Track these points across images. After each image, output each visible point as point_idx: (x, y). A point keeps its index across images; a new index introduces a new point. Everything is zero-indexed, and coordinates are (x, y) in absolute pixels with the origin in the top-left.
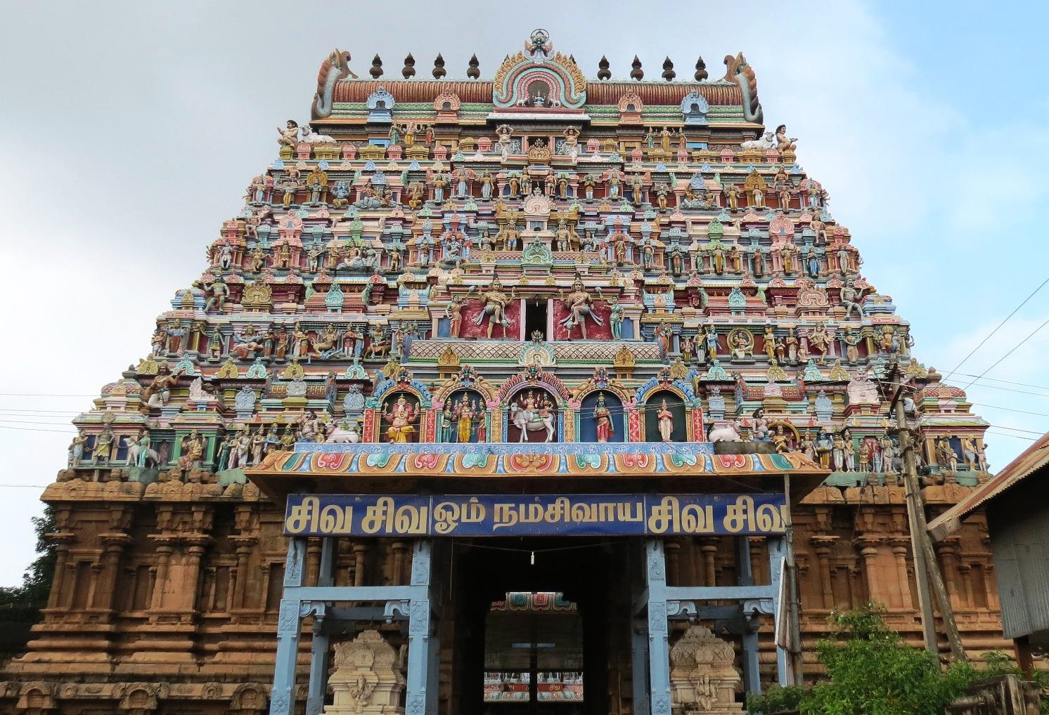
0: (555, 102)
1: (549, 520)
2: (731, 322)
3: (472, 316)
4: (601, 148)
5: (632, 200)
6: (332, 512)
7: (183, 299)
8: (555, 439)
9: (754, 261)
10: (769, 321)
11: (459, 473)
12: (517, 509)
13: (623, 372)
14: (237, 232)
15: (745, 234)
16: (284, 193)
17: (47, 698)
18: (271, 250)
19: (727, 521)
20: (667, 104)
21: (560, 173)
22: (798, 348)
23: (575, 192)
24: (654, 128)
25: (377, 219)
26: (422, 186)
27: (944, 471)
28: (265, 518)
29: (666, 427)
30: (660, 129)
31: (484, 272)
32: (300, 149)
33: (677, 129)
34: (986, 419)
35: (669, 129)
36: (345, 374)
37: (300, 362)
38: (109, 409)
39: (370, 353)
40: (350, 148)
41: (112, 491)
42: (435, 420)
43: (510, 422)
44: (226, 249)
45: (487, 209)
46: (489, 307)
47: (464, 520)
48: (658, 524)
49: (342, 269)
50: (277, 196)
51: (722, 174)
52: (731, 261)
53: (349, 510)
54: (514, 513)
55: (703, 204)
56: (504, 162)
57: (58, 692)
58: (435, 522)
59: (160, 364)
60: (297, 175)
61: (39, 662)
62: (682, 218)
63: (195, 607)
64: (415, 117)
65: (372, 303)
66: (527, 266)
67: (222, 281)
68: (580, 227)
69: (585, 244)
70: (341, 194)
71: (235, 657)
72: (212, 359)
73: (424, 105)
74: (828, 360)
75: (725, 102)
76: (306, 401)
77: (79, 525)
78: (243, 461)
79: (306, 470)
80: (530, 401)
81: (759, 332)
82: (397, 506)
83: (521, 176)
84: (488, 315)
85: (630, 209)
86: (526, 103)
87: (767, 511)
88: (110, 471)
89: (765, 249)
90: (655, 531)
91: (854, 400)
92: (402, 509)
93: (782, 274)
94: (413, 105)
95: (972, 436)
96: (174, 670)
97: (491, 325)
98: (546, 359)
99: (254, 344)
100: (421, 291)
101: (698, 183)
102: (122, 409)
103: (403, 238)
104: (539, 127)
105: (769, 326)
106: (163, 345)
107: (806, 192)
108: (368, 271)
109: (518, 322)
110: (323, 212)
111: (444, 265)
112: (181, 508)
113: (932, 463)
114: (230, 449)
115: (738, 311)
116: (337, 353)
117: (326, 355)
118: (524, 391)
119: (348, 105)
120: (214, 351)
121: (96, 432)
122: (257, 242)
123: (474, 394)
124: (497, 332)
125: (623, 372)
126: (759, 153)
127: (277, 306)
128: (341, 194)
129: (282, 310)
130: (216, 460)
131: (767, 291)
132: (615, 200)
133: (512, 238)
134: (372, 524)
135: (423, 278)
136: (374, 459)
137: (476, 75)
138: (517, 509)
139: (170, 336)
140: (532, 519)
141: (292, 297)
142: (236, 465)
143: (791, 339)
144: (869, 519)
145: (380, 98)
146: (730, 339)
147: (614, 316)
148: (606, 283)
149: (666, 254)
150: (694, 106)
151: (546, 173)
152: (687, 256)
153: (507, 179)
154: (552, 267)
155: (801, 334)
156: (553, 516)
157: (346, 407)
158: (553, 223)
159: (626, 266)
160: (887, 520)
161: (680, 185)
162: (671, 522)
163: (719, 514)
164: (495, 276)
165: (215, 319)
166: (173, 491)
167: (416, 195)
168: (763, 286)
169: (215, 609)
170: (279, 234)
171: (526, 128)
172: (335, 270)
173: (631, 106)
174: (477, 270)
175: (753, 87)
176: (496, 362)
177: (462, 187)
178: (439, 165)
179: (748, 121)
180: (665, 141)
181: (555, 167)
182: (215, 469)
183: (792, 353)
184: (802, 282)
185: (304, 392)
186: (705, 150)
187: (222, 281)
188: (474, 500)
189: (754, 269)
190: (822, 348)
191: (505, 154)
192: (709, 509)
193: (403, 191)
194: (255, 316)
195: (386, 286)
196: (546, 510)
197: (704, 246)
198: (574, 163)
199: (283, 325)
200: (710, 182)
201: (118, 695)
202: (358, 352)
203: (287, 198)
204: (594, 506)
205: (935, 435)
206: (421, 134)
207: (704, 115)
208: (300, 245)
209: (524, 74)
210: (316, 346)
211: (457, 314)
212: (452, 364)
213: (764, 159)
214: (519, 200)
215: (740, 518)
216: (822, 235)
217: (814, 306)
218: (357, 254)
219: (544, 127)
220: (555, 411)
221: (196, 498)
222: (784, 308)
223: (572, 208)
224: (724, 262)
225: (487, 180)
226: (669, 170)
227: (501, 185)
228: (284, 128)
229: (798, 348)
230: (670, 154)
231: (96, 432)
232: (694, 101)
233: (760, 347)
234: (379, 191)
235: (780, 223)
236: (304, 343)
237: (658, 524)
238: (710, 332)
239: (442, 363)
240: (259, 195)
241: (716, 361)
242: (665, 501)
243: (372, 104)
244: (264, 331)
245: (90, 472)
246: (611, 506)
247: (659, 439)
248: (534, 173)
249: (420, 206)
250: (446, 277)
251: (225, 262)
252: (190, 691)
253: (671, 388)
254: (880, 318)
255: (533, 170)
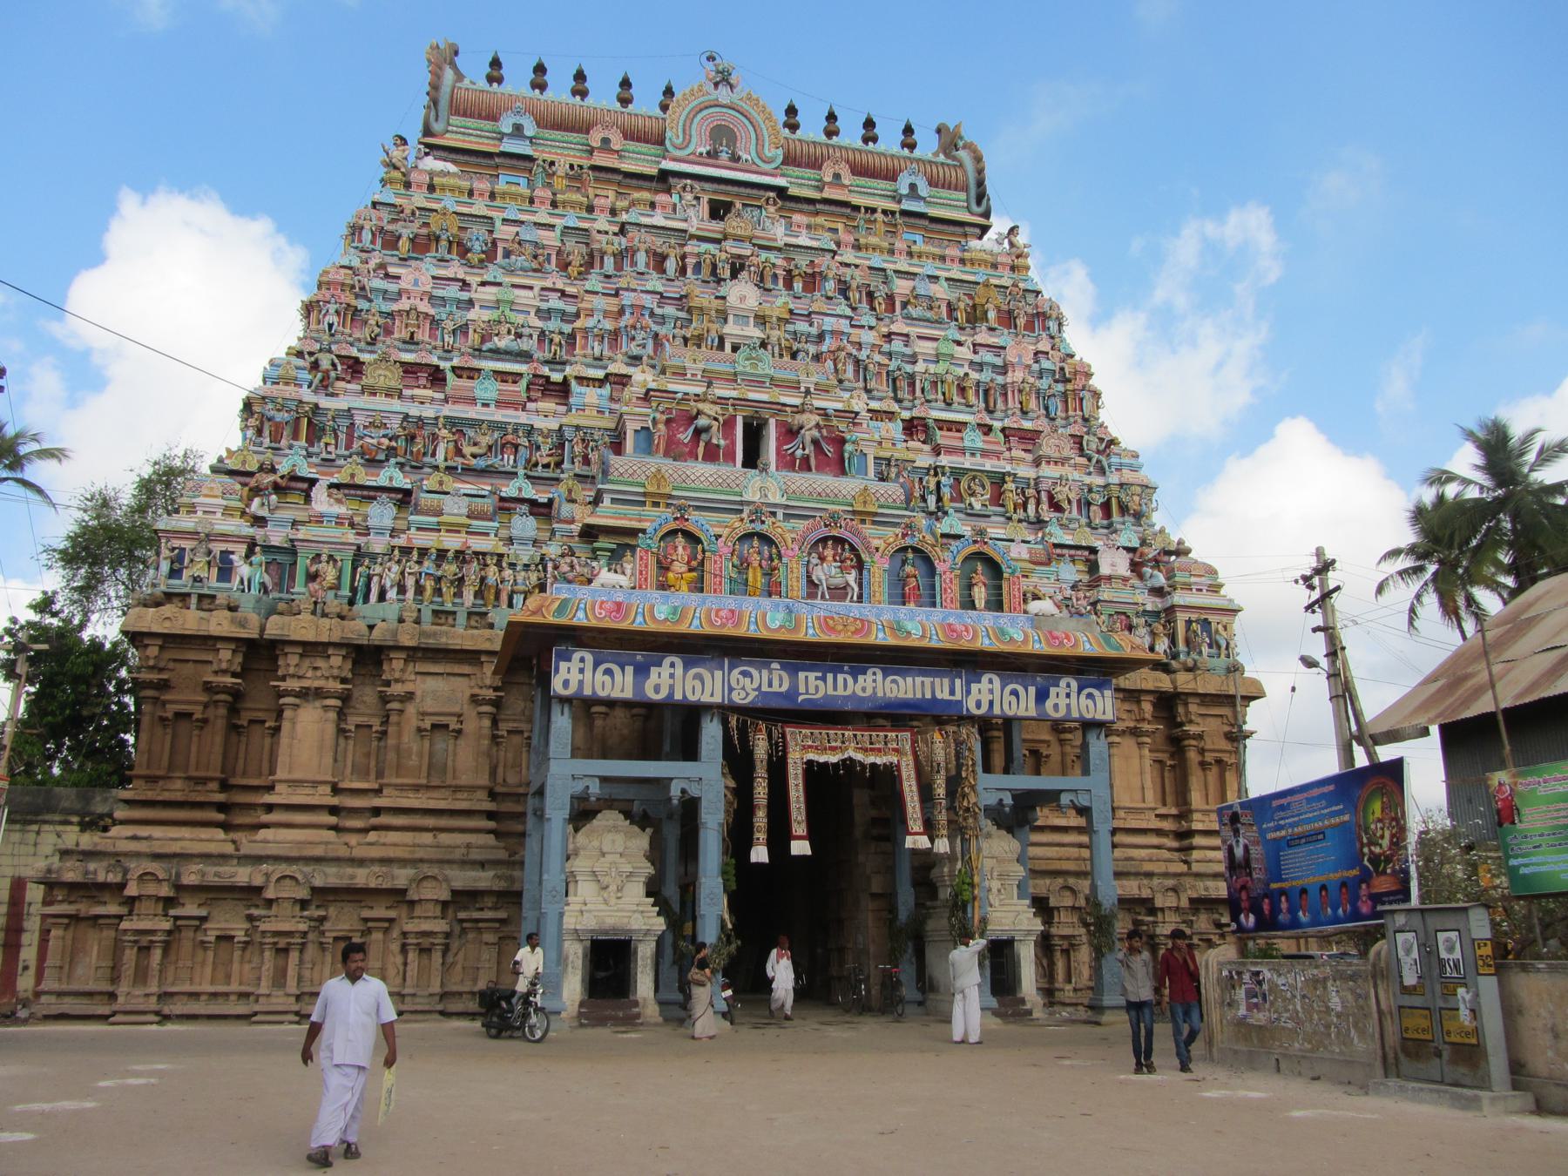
0: (744, 156)
1: (861, 694)
2: (967, 465)
3: (684, 432)
4: (809, 227)
5: (847, 299)
6: (608, 672)
7: (281, 372)
8: (860, 597)
9: (986, 392)
10: (1008, 468)
11: (765, 634)
12: (824, 679)
13: (863, 516)
14: (343, 284)
15: (977, 358)
16: (399, 237)
17: (165, 884)
18: (391, 315)
19: (1049, 704)
20: (471, 116)
21: (764, 255)
22: (1038, 503)
23: (781, 282)
24: (867, 209)
25: (531, 288)
26: (584, 249)
27: (1194, 655)
28: (421, 667)
29: (980, 594)
30: (874, 211)
31: (690, 375)
32: (414, 177)
33: (893, 213)
34: (1238, 601)
35: (885, 212)
36: (510, 489)
37: (450, 470)
38: (200, 514)
39: (536, 465)
40: (482, 185)
41: (219, 624)
42: (721, 564)
43: (809, 576)
44: (332, 308)
45: (673, 291)
46: (702, 422)
47: (765, 688)
48: (978, 705)
49: (490, 351)
50: (391, 242)
51: (947, 279)
52: (962, 390)
53: (629, 670)
54: (820, 683)
55: (929, 314)
56: (693, 231)
57: (178, 875)
58: (731, 689)
59: (261, 457)
60: (413, 214)
61: (135, 838)
62: (905, 330)
63: (223, 772)
64: (563, 152)
65: (530, 399)
66: (743, 374)
67: (330, 351)
68: (790, 327)
69: (798, 351)
70: (477, 247)
71: (393, 837)
72: (324, 455)
73: (573, 137)
74: (1070, 520)
75: (947, 185)
76: (469, 521)
77: (171, 665)
78: (392, 594)
79: (580, 619)
80: (829, 553)
81: (999, 480)
82: (686, 667)
83: (717, 252)
84: (698, 432)
85: (848, 312)
86: (708, 153)
87: (1090, 696)
88: (213, 597)
89: (1000, 379)
90: (975, 712)
91: (1105, 570)
92: (890, 678)
93: (1018, 413)
94: (557, 135)
95: (1225, 619)
96: (318, 851)
97: (702, 444)
98: (774, 495)
99: (386, 441)
100: (599, 391)
101: (924, 288)
102: (219, 515)
103: (565, 317)
104: (723, 187)
105: (1009, 474)
106: (259, 432)
107: (1044, 314)
108: (525, 356)
109: (733, 443)
110: (456, 269)
111: (626, 359)
112: (312, 649)
113: (1182, 647)
114: (370, 578)
115: (973, 453)
116: (493, 461)
117: (481, 463)
118: (824, 540)
119: (470, 122)
120: (327, 444)
121: (188, 545)
122: (370, 301)
123: (765, 539)
124: (712, 455)
125: (863, 516)
126: (988, 257)
127: (407, 392)
128: (477, 247)
129: (412, 397)
130: (354, 590)
131: (1003, 430)
132: (830, 298)
133: (713, 334)
134: (657, 689)
135: (600, 374)
136: (662, 612)
137: (583, 94)
138: (824, 679)
139: (269, 420)
140: (840, 692)
141: (423, 382)
142: (382, 597)
143: (1031, 492)
144: (293, 660)
145: (606, 134)
146: (964, 484)
147: (848, 447)
148: (840, 406)
149: (1038, 392)
150: (913, 187)
151: (748, 253)
152: (911, 378)
153: (698, 255)
154: (772, 379)
155: (1043, 486)
156: (864, 689)
157: (515, 533)
158: (761, 320)
159: (846, 384)
160: (1134, 707)
161: (901, 287)
162: (991, 703)
163: (1042, 696)
164: (709, 385)
165: (325, 402)
166: (303, 628)
167: (576, 260)
168: (997, 425)
169: (244, 774)
170: (400, 294)
171: (707, 186)
172: (480, 350)
173: (837, 176)
174: (681, 373)
175: (980, 171)
176: (715, 492)
177: (641, 258)
178: (602, 222)
179: (972, 214)
180: (881, 228)
181: (761, 247)
182: (351, 602)
183: (1031, 508)
184: (1042, 424)
185: (465, 511)
186: (920, 246)
187: (330, 351)
188: (775, 665)
189: (986, 401)
190: (1065, 505)
191: (695, 222)
192: (1032, 690)
193: (559, 253)
194: (380, 403)
195: (548, 378)
196: (856, 681)
197: (932, 368)
198: (780, 244)
199: (420, 418)
200: (933, 286)
201: (258, 881)
202: (522, 462)
203: (404, 244)
204: (909, 680)
205: (1186, 616)
206: (576, 177)
207: (924, 199)
208: (432, 311)
209: (705, 113)
210: (467, 450)
211: (661, 427)
212: (662, 491)
213: (995, 266)
214: (713, 285)
215: (1063, 702)
216: (1062, 369)
217: (1057, 455)
218: (509, 332)
219: (729, 188)
220: (860, 566)
221: (336, 638)
222: (1023, 454)
223: (780, 301)
224: (954, 390)
225: (672, 253)
226: (885, 265)
227: (691, 261)
228: (389, 143)
229: (1038, 503)
230: (885, 245)
231: (188, 545)
232: (912, 179)
233: (997, 499)
234: (529, 249)
235: (1019, 349)
236: (451, 445)
237: (978, 705)
238: (944, 474)
239: (651, 489)
240: (367, 236)
241: (951, 511)
242: (985, 678)
243: (506, 126)
244: (395, 424)
245: (184, 597)
246: (928, 680)
247: (973, 607)
248: (734, 251)
249: (582, 276)
250: (643, 377)
251: (331, 326)
252: (353, 877)
253: (985, 549)
254: (1128, 476)
255: (731, 247)
